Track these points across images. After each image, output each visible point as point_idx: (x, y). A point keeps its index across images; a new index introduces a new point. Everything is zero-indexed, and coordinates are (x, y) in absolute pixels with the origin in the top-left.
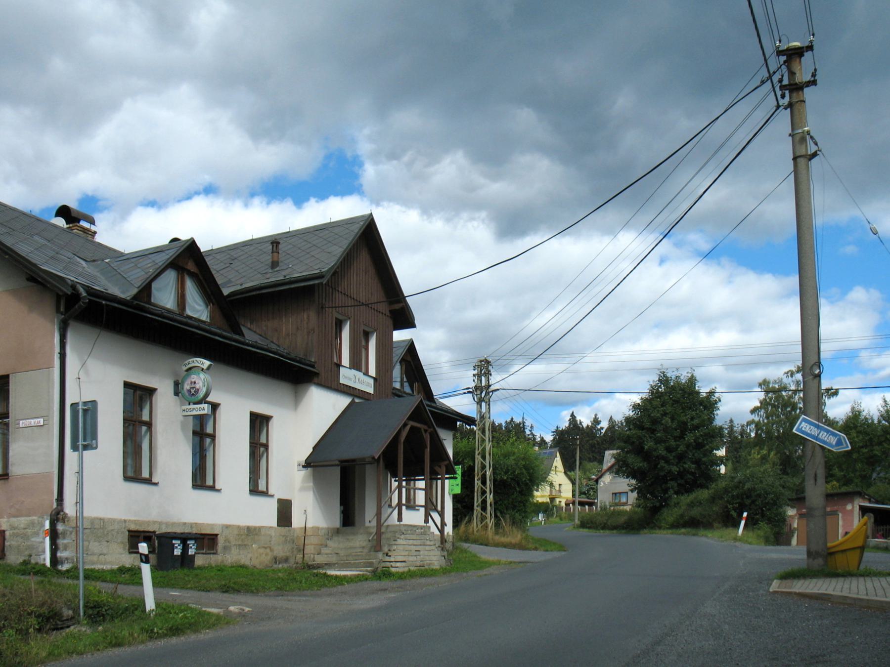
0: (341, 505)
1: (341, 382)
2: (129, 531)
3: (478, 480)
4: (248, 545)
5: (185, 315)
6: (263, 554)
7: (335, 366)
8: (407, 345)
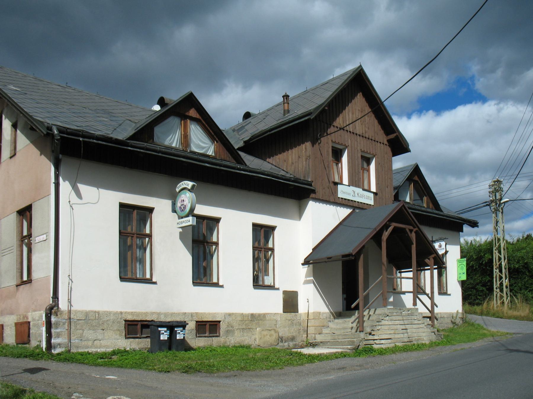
0: (343, 293)
1: (339, 196)
2: (126, 321)
3: (496, 269)
4: (253, 329)
5: (189, 151)
6: (267, 335)
7: (333, 184)
8: (412, 168)
